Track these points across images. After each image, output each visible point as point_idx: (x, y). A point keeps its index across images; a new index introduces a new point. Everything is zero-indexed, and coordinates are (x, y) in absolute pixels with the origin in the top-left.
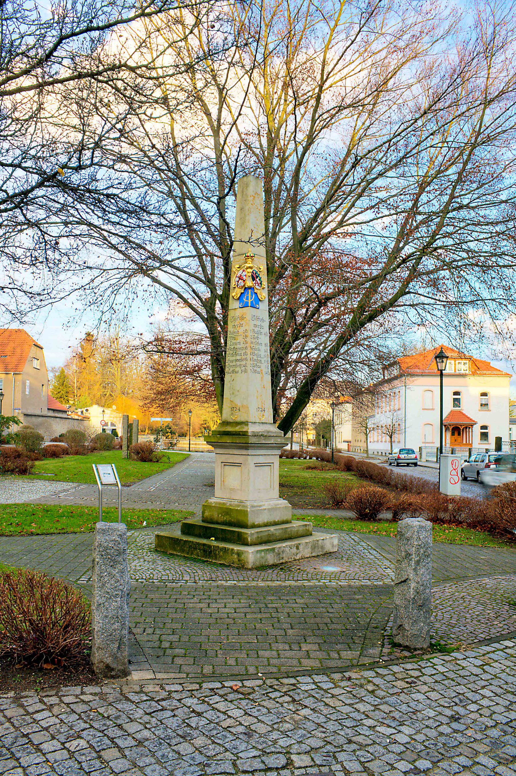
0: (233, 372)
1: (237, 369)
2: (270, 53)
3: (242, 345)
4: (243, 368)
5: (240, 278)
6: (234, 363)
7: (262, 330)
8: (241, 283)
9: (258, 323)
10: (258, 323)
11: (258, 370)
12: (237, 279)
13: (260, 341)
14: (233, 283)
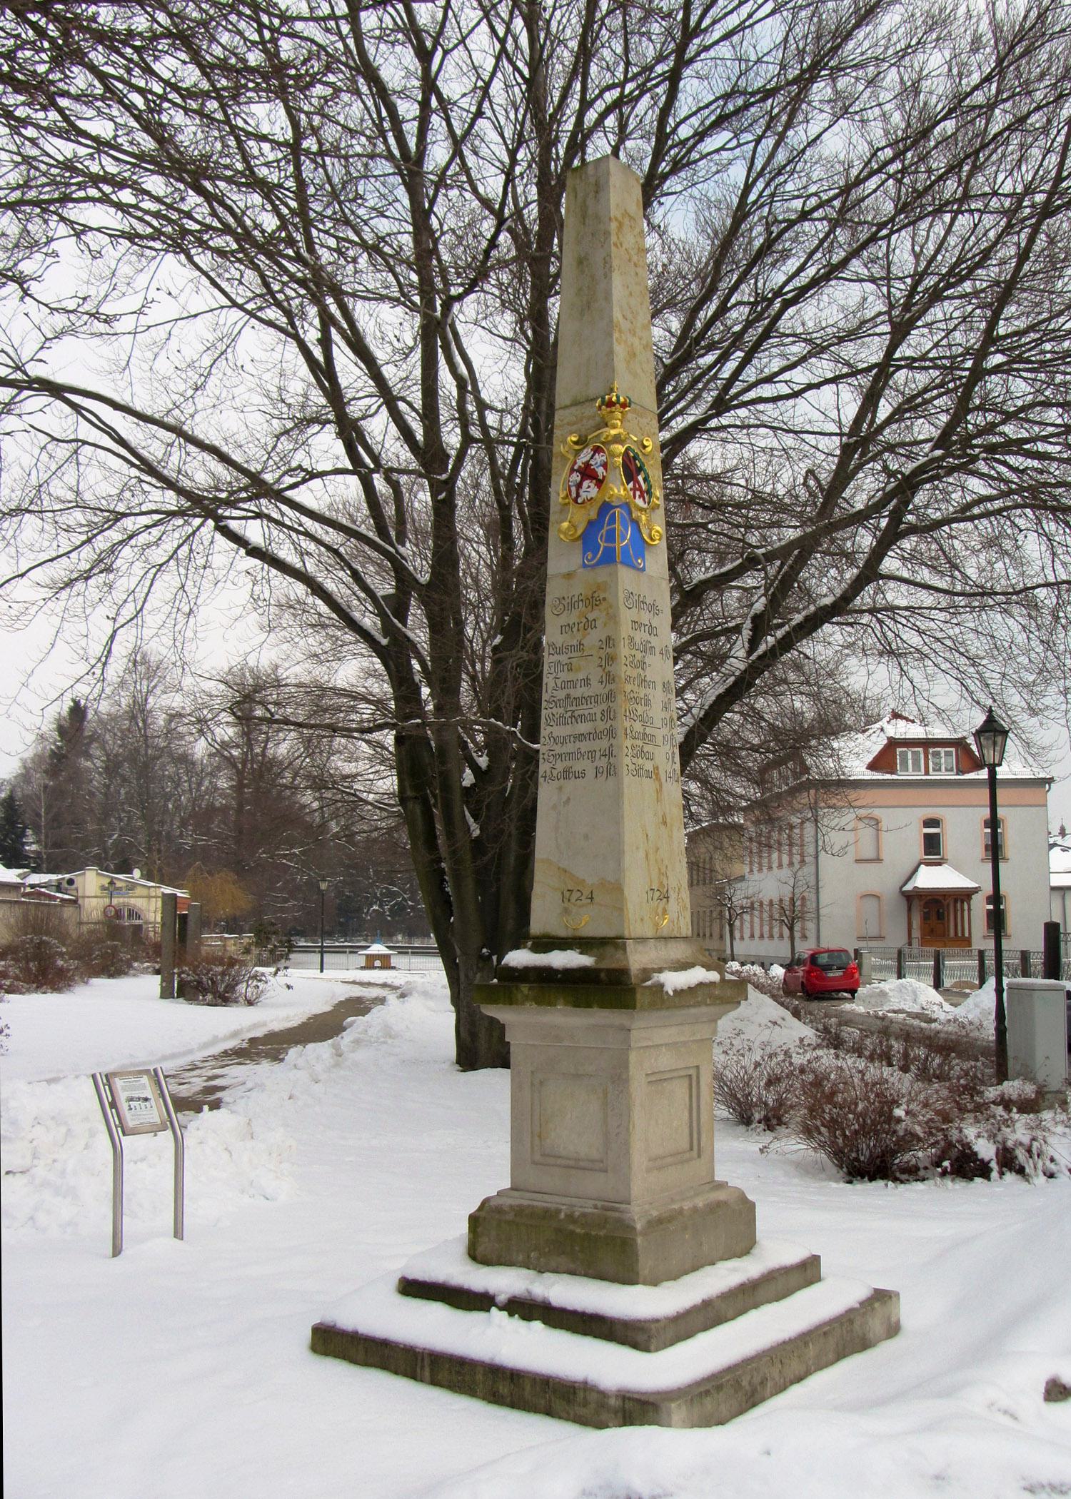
0: (567, 774)
1: (578, 766)
2: (1027, 421)
3: (596, 688)
4: (603, 762)
5: (587, 473)
6: (570, 748)
7: (655, 641)
8: (589, 489)
9: (645, 617)
10: (645, 617)
11: (649, 766)
12: (576, 477)
13: (650, 675)
14: (558, 491)
